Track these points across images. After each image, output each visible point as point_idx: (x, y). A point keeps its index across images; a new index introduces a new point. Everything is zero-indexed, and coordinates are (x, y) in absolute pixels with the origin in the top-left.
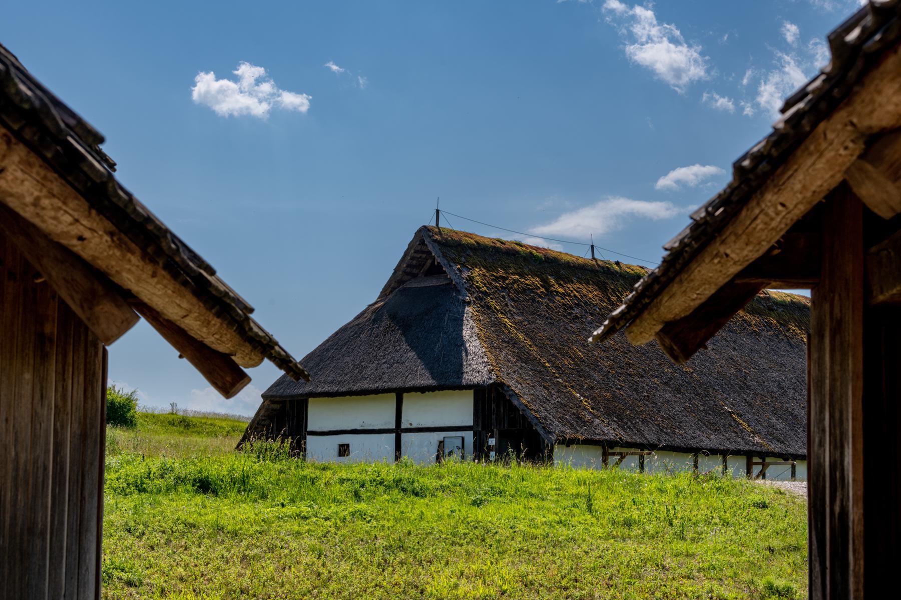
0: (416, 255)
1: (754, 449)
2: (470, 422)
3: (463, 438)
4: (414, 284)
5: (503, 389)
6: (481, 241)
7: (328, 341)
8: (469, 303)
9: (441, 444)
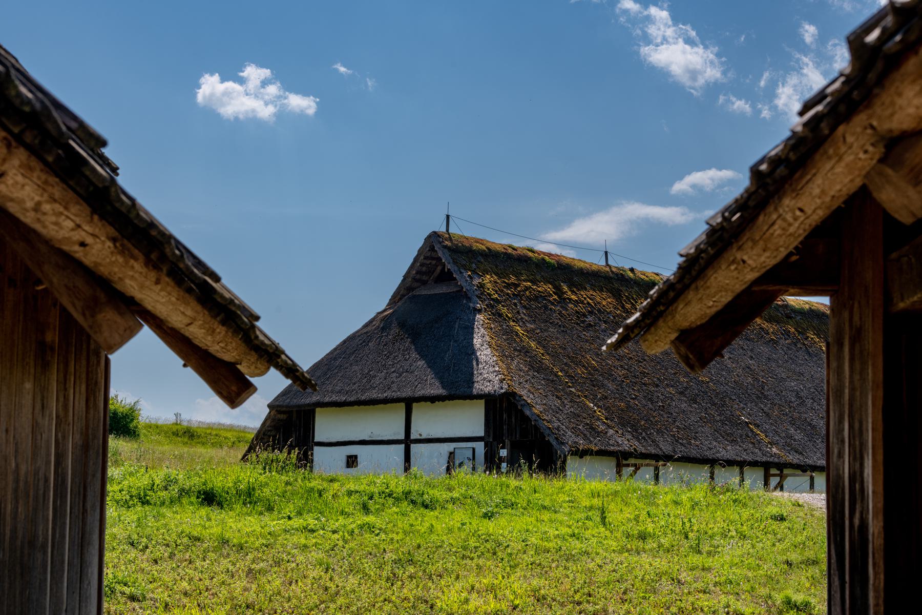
0: (425, 261)
1: (771, 460)
2: (481, 433)
3: (474, 449)
4: (424, 292)
5: (515, 399)
6: (492, 247)
7: (335, 349)
8: (480, 311)
9: (452, 455)
